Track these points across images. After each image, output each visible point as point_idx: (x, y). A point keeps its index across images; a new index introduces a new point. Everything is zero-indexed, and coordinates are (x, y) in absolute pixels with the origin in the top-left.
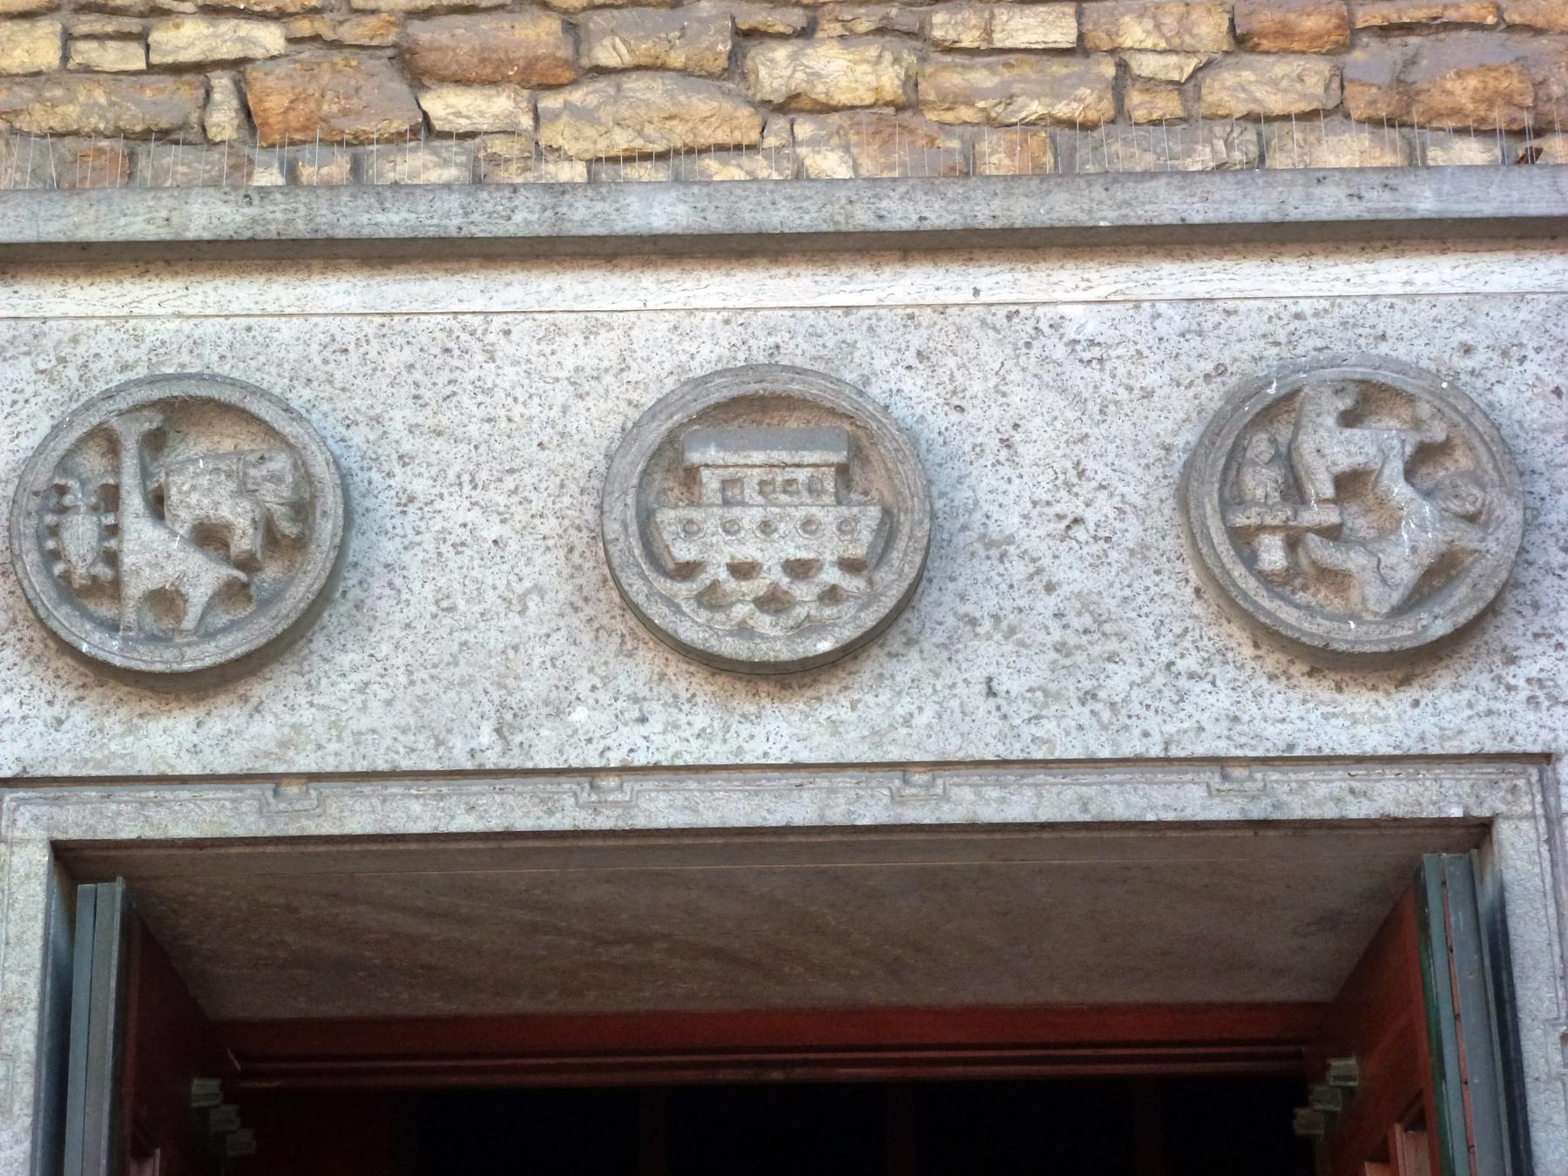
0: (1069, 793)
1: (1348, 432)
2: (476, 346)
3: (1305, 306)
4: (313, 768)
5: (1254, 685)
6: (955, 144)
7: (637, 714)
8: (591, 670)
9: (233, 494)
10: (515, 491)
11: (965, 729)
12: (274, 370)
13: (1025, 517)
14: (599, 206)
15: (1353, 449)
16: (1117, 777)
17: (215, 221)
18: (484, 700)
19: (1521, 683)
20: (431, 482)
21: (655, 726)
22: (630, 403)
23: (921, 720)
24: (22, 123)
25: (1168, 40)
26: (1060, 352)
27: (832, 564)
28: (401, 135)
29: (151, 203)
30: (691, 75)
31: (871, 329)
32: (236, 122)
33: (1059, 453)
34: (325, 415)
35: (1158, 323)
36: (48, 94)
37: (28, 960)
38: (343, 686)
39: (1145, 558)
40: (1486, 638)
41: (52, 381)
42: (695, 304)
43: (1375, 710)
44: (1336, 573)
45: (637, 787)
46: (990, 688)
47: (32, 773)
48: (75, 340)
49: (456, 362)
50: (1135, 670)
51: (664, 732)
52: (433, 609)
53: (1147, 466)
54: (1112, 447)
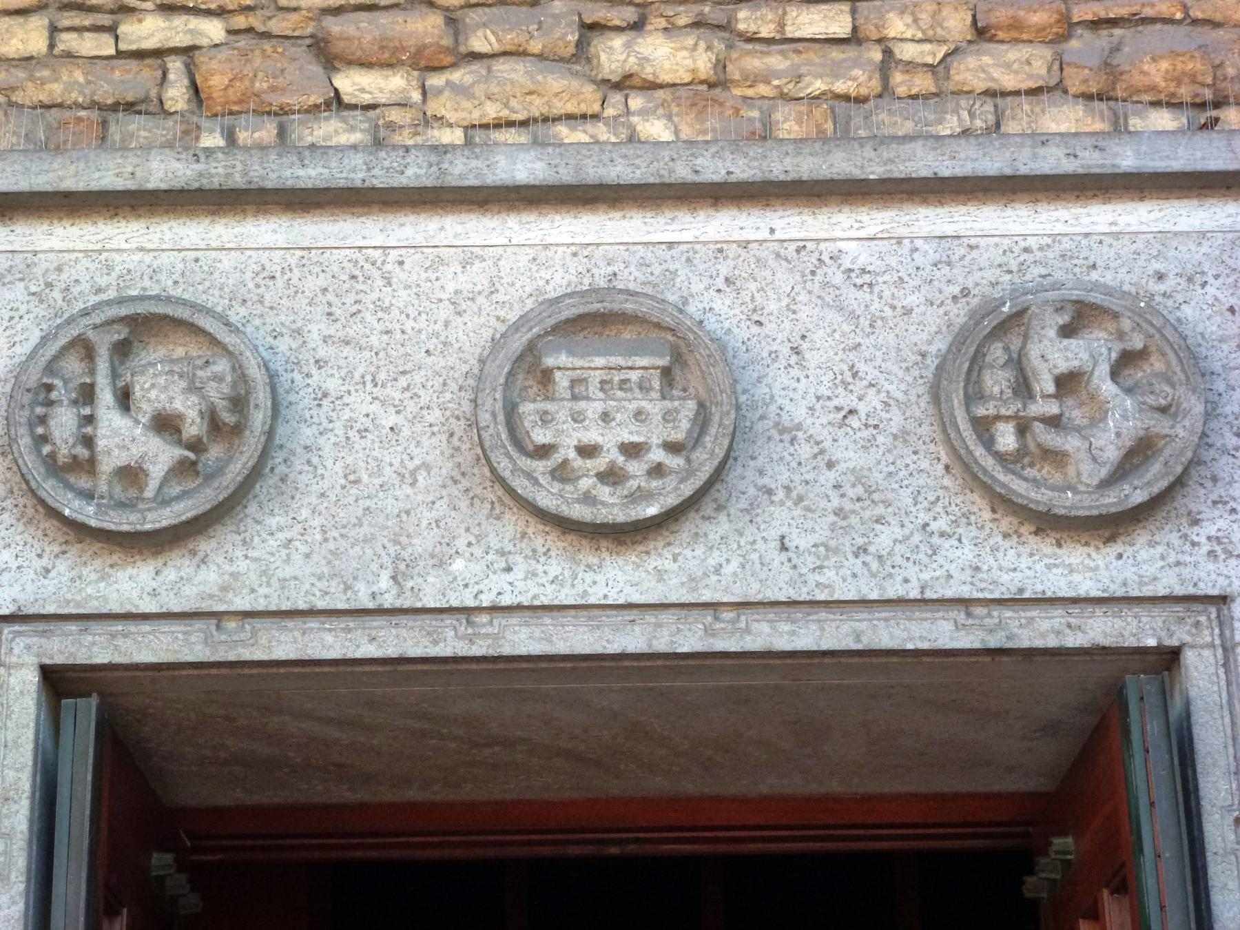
0: (846, 627)
1: (1066, 342)
2: (376, 274)
3: (1032, 242)
4: (248, 608)
5: (992, 542)
6: (755, 114)
7: (503, 565)
8: (467, 530)
9: (184, 391)
10: (407, 388)
11: (763, 576)
12: (216, 293)
13: (811, 409)
14: (474, 163)
15: (1070, 355)
16: (884, 615)
17: (170, 175)
18: (383, 554)
19: (1203, 540)
20: (341, 381)
21: (518, 573)
22: (498, 318)
23: (728, 570)
24: (17, 97)
25: (923, 32)
26: (838, 278)
27: (658, 446)
28: (317, 106)
29: (119, 161)
30: (546, 59)
31: (688, 260)
32: (186, 96)
33: (837, 358)
34: (257, 328)
35: (916, 256)
36: (38, 75)
37: (22, 760)
38: (271, 542)
39: (905, 441)
40: (1175, 504)
41: (41, 301)
42: (549, 240)
43: (1087, 561)
44: (1057, 453)
45: (504, 622)
46: (783, 544)
47: (25, 611)
48: (59, 269)
49: (360, 287)
50: (897, 530)
51: (525, 579)
52: (343, 481)
53: (907, 369)
54: (879, 354)
